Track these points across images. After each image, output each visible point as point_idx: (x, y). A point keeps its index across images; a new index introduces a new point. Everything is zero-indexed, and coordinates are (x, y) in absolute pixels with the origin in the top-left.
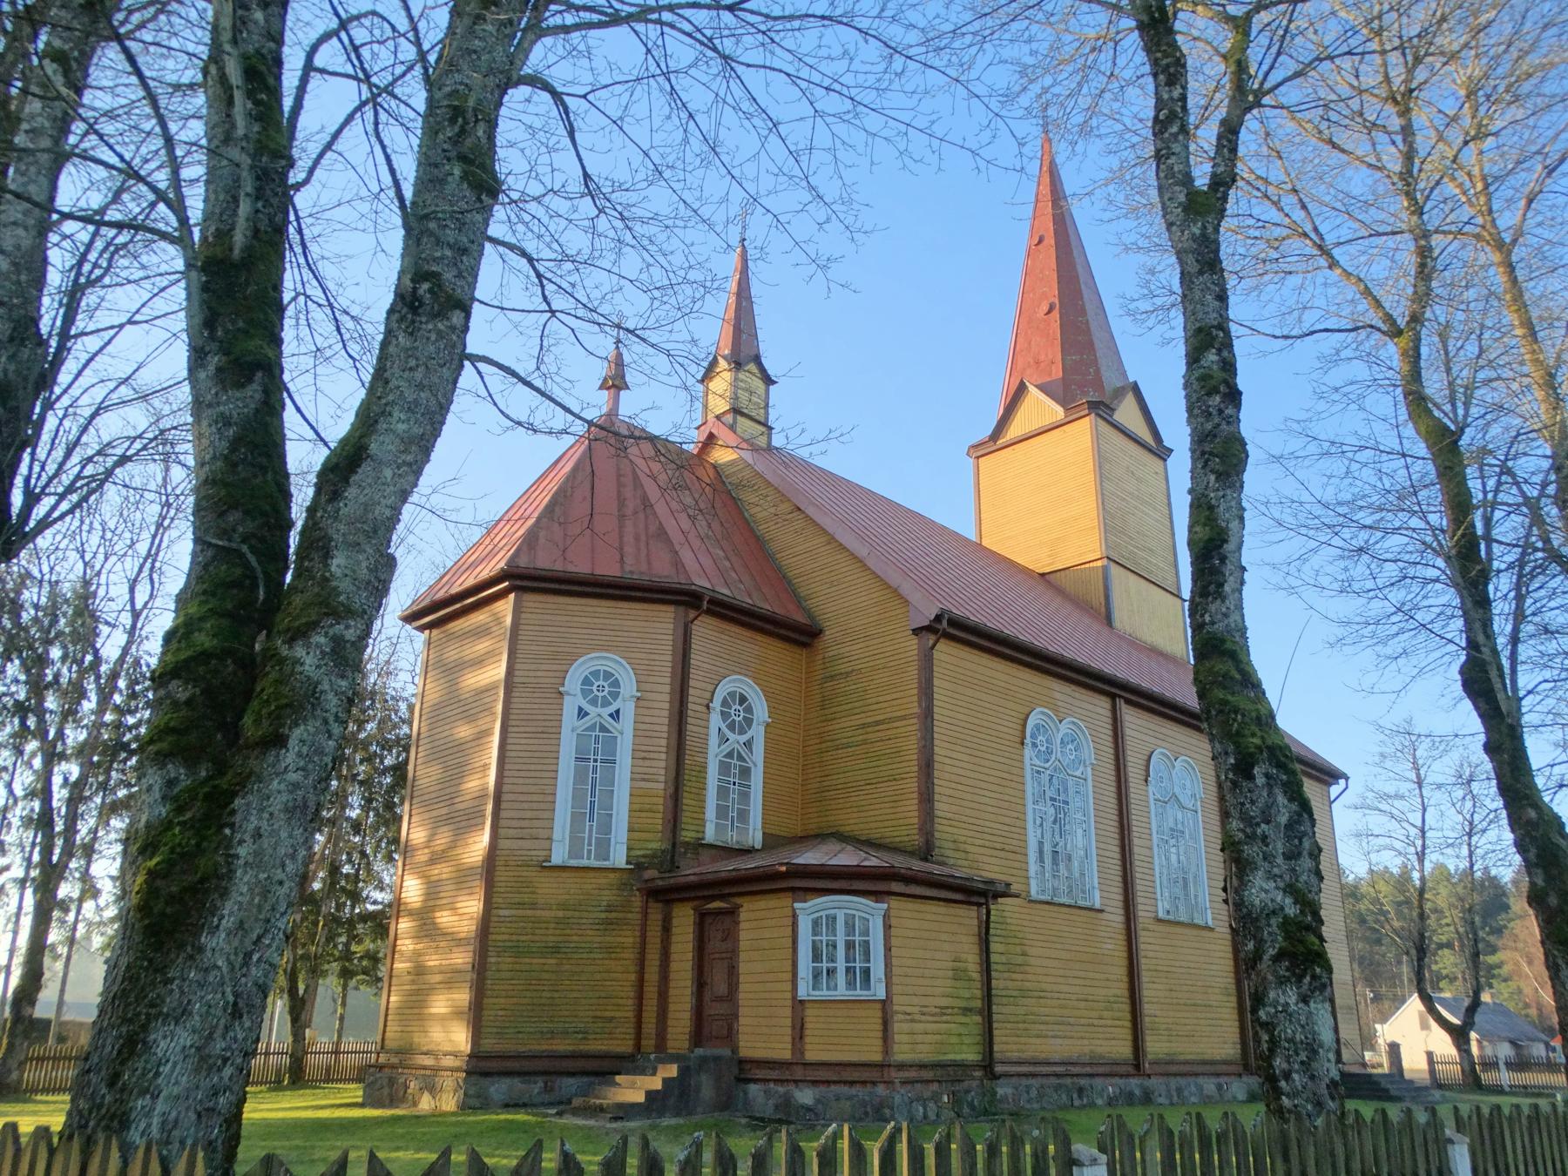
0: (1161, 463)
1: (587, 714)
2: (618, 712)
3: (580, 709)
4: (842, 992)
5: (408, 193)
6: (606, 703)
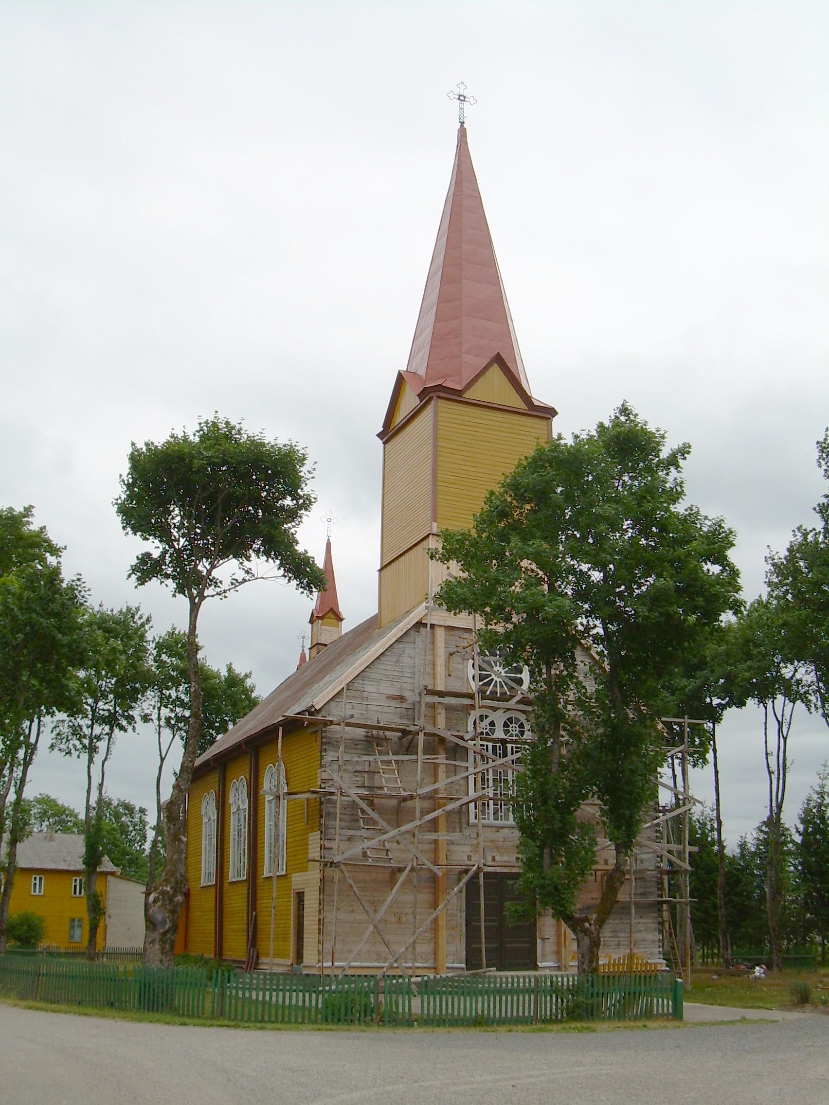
0: (544, 423)
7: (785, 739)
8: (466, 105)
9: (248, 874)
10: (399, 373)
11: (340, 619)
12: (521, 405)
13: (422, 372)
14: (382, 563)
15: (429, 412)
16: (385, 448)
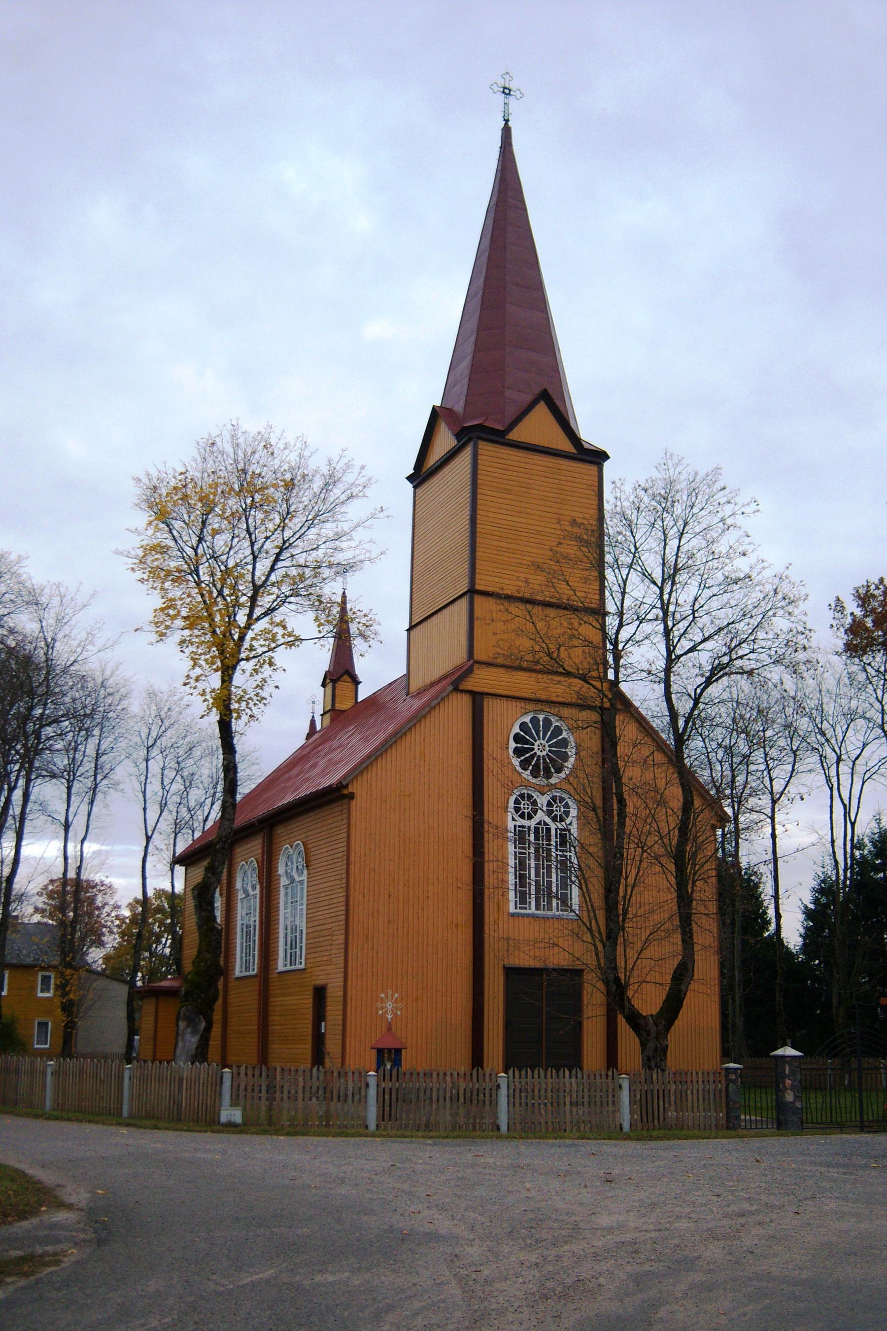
0: (595, 468)
7: (853, 824)
8: (511, 100)
9: (260, 968)
10: (434, 407)
11: (356, 682)
12: (567, 446)
13: (459, 408)
14: (411, 622)
15: (466, 456)
16: (415, 493)
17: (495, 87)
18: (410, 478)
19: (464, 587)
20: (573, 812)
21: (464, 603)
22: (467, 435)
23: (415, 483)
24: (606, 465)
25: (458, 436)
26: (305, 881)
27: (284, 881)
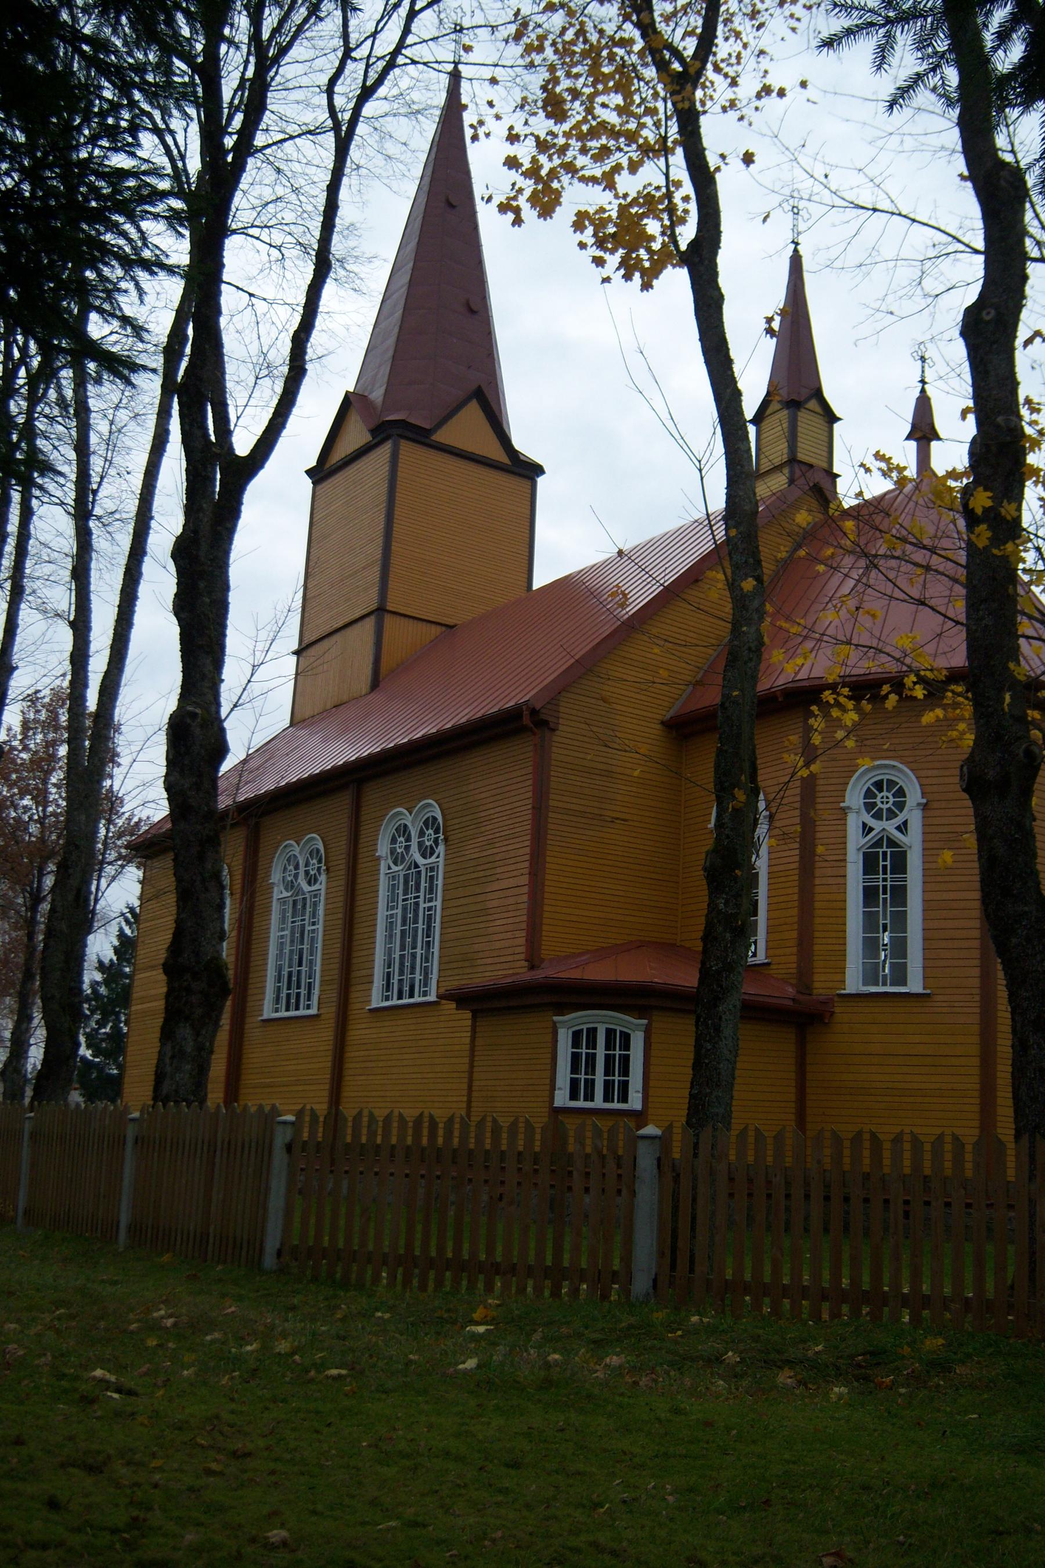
0: (529, 483)
1: (871, 829)
2: (905, 823)
3: (864, 825)
4: (598, 1102)
5: (1028, 205)
6: (891, 815)
12: (504, 459)
13: (377, 395)
17: (931, 364)
18: (309, 472)
19: (369, 600)
20: (914, 796)
21: (369, 624)
22: (383, 432)
23: (317, 477)
24: (540, 480)
25: (374, 431)
26: (323, 892)
27: (279, 893)
